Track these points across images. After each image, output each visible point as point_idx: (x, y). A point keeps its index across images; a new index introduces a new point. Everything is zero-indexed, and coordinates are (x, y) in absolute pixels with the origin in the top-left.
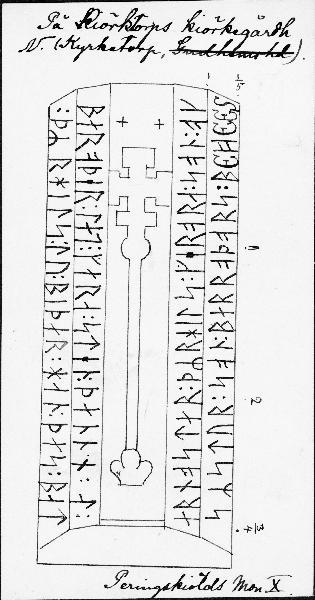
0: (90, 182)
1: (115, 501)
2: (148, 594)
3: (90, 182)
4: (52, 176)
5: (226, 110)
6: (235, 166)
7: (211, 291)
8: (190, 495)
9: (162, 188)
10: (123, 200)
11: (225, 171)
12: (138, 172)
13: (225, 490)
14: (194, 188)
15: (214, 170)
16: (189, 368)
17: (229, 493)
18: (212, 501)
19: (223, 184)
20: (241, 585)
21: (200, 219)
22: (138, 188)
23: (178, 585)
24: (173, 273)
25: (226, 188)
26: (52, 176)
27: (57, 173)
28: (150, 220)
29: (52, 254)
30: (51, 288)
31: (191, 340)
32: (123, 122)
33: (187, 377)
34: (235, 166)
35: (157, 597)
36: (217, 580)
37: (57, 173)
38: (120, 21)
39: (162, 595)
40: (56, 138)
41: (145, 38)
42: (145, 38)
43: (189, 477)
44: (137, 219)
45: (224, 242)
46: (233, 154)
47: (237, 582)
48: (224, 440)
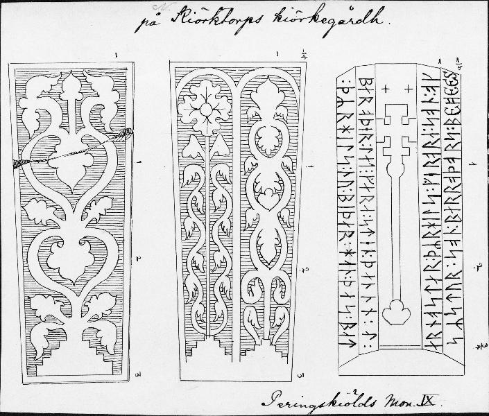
0: (367, 129)
1: (388, 335)
2: (306, 411)
3: (367, 129)
4: (340, 125)
5: (450, 79)
6: (458, 113)
7: (445, 196)
8: (436, 329)
9: (410, 131)
10: (387, 139)
11: (452, 117)
12: (396, 120)
13: (457, 324)
14: (424, 130)
15: (445, 118)
16: (433, 248)
17: (461, 326)
18: (451, 332)
19: (450, 127)
20: (392, 401)
21: (438, 151)
22: (396, 130)
23: (333, 403)
24: (421, 186)
25: (453, 128)
26: (340, 125)
27: (345, 123)
28: (406, 151)
29: (341, 177)
30: (343, 198)
31: (433, 230)
32: (386, 89)
33: (369, 265)
34: (458, 113)
35: (313, 413)
36: (371, 398)
37: (345, 123)
38: (210, 15)
39: (318, 411)
40: (343, 102)
41: (328, 32)
42: (328, 32)
43: (435, 318)
44: (396, 150)
45: (453, 164)
46: (456, 105)
47: (389, 399)
48: (455, 293)
